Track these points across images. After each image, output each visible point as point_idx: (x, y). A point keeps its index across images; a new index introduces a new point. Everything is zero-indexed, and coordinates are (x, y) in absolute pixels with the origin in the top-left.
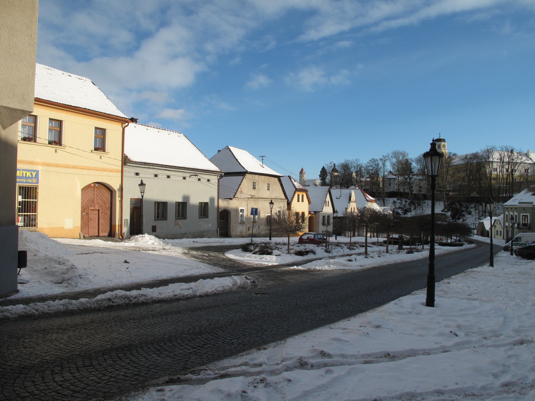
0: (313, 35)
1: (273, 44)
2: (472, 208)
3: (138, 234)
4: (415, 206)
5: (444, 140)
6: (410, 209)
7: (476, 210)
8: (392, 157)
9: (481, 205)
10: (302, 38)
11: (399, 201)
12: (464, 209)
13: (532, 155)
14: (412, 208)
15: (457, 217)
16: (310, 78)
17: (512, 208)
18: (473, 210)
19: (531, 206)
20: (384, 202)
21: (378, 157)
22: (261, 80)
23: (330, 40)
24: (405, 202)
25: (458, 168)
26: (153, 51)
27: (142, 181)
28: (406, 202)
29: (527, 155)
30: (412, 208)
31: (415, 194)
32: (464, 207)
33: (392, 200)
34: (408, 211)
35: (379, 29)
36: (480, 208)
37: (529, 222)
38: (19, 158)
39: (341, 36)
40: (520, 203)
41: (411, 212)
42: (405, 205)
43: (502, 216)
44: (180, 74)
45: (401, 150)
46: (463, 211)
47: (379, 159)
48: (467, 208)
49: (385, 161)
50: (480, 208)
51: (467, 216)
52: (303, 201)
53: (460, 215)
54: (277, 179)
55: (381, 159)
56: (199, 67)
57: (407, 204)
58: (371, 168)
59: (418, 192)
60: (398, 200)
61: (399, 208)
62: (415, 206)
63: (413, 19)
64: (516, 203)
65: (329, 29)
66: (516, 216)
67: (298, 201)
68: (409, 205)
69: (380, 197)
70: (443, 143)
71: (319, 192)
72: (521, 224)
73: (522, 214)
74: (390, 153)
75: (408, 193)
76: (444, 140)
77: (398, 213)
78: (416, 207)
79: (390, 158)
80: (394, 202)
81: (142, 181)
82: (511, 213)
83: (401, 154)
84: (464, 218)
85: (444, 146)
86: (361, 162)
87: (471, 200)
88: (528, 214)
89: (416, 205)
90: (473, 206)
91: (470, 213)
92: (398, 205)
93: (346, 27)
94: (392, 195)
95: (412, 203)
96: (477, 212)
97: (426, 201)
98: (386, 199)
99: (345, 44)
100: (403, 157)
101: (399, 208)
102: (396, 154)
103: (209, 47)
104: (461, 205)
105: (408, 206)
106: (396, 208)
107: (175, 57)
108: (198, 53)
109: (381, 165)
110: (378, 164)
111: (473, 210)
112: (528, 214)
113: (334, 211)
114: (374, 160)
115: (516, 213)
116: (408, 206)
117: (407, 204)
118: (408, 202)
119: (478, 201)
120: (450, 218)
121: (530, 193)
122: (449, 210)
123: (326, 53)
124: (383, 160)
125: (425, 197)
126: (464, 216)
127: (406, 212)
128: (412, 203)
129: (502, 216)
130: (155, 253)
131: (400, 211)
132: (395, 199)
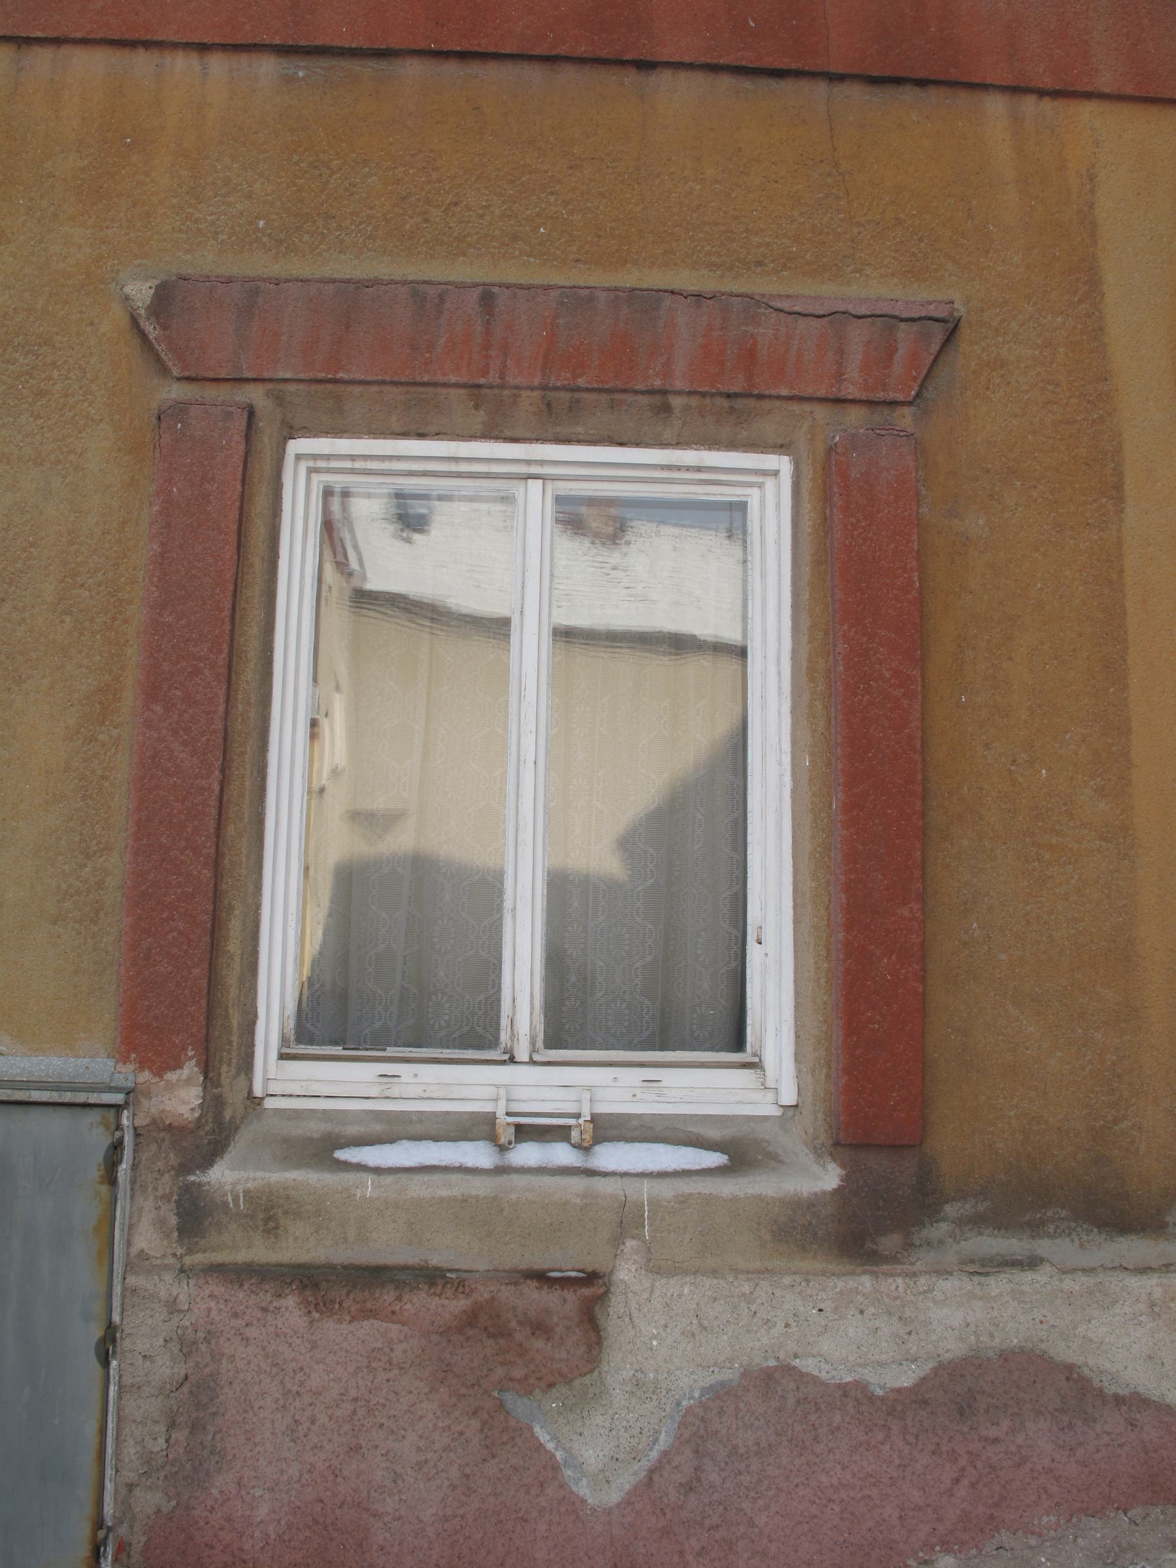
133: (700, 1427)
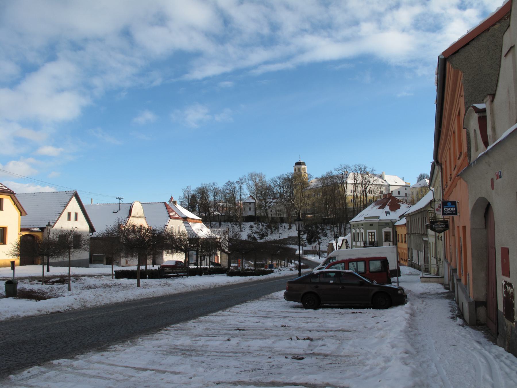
0: (197, 74)
1: (158, 82)
2: (328, 230)
4: (271, 229)
5: (304, 164)
6: (267, 233)
7: (331, 232)
8: (248, 179)
9: (337, 226)
10: (188, 77)
11: (256, 225)
12: (320, 231)
13: (386, 177)
14: (269, 232)
15: (312, 240)
16: (195, 115)
17: (360, 225)
18: (328, 232)
19: (376, 221)
20: (240, 226)
22: (148, 116)
23: (213, 81)
24: (262, 226)
25: (316, 190)
26: (38, 84)
27: (49, 223)
28: (263, 226)
29: (381, 177)
30: (269, 232)
31: (272, 218)
32: (320, 229)
33: (249, 224)
34: (265, 236)
35: (259, 71)
36: (335, 229)
37: (376, 240)
39: (224, 76)
40: (366, 218)
41: (267, 236)
42: (261, 230)
43: (349, 235)
44: (65, 107)
45: (258, 172)
46: (319, 234)
47: (235, 182)
48: (323, 229)
49: (242, 183)
50: (335, 229)
51: (323, 238)
52: (76, 219)
53: (316, 238)
55: (237, 182)
56: (85, 101)
57: (264, 228)
58: (228, 192)
60: (255, 224)
61: (256, 232)
62: (271, 229)
63: (289, 65)
64: (362, 219)
65: (212, 70)
66: (362, 233)
67: (69, 219)
68: (266, 229)
69: (238, 222)
70: (303, 167)
72: (368, 242)
73: (368, 231)
74: (247, 177)
76: (304, 164)
77: (254, 238)
78: (273, 231)
79: (247, 180)
80: (251, 227)
81: (49, 223)
82: (358, 231)
84: (320, 240)
85: (304, 169)
86: (218, 186)
87: (326, 222)
88: (375, 231)
89: (273, 228)
90: (328, 227)
91: (326, 235)
92: (255, 229)
93: (228, 69)
94: (249, 219)
95: (269, 227)
96: (333, 233)
97: (283, 225)
98: (244, 223)
99: (228, 84)
100: (261, 179)
101: (256, 232)
102: (252, 177)
103: (97, 81)
104: (317, 227)
105: (264, 231)
106: (253, 233)
107: (61, 90)
108: (85, 87)
109: (237, 188)
110: (235, 188)
111: (328, 232)
112: (375, 231)
113: (92, 229)
114: (230, 183)
115: (362, 231)
116: (264, 231)
117: (264, 228)
118: (265, 226)
119: (334, 222)
120: (306, 241)
121: (378, 207)
122: (305, 233)
123: (207, 91)
124: (240, 183)
125: (282, 220)
126: (319, 238)
127: (262, 236)
128: (269, 227)
129: (349, 235)
131: (256, 236)
132: (252, 223)
133: (292, 249)
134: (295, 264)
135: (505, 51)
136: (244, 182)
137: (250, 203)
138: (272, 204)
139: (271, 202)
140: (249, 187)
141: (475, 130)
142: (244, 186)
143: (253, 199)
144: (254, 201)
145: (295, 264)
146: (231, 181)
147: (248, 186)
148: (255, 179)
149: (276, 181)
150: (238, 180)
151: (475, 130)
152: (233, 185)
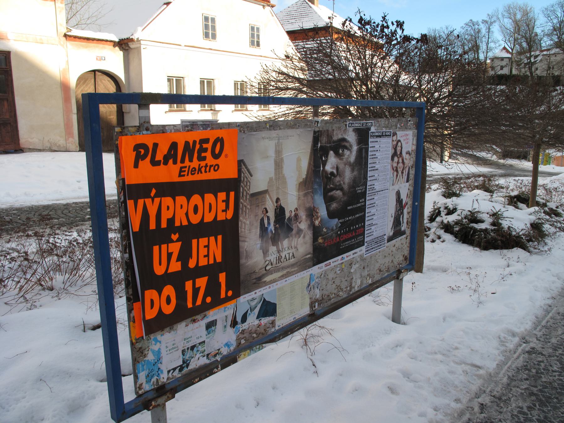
3: (151, 333)
8: (503, 16)
21: (479, 16)
31: (540, 78)
38: (106, 193)
49: (492, 23)
54: (206, 254)
55: (485, 22)
59: (544, 74)
71: (403, 63)
74: (501, 10)
75: (526, 77)
79: (500, 16)
83: (520, 9)
102: (510, 11)
109: (484, 31)
110: (479, 31)
114: (472, 23)
124: (489, 24)
130: (227, 114)
134: (373, 56)
135: (414, 166)
136: (495, 22)
137: (502, 59)
138: (539, 58)
139: (536, 57)
140: (503, 28)
141: (160, 264)
142: (495, 28)
143: (508, 51)
144: (509, 56)
145: (373, 56)
146: (475, 20)
147: (501, 27)
148: (515, 15)
149: (554, 11)
150: (485, 19)
151: (160, 264)
152: (477, 27)
